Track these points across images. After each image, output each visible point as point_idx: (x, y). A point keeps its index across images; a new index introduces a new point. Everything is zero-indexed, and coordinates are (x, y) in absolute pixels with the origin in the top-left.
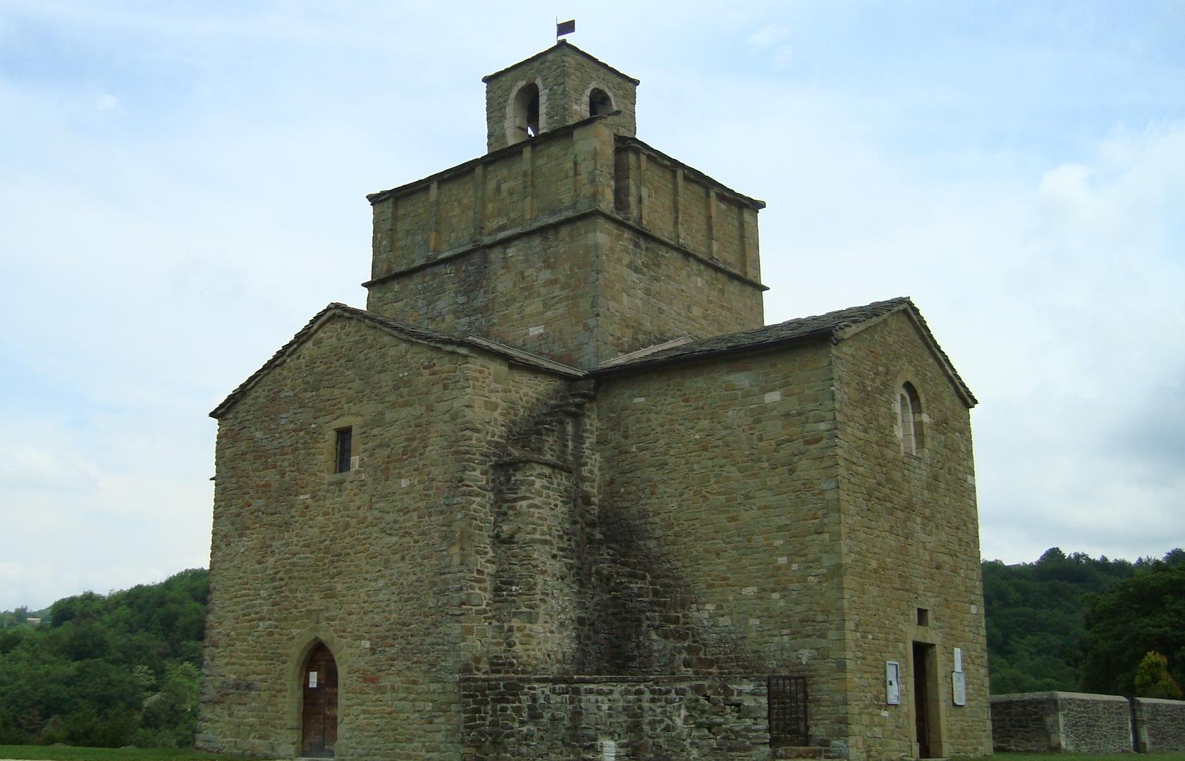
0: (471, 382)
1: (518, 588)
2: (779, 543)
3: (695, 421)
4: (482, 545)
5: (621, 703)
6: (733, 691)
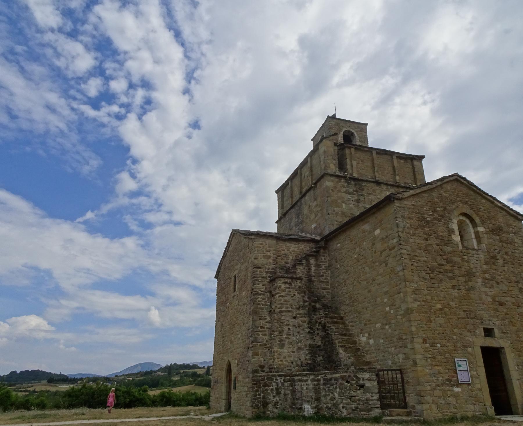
0: (256, 249)
2: (385, 300)
4: (263, 316)
6: (360, 378)
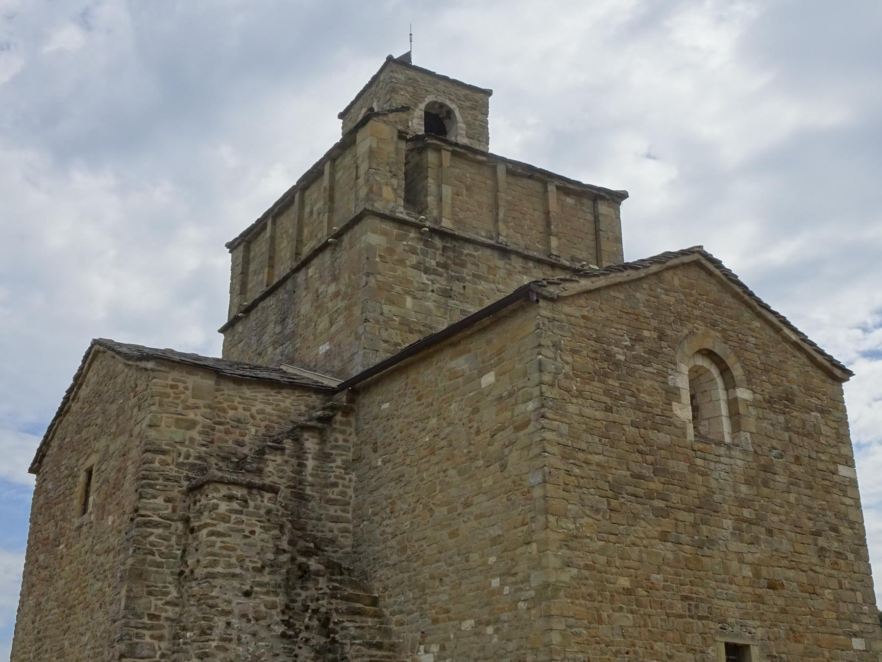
4: (160, 585)
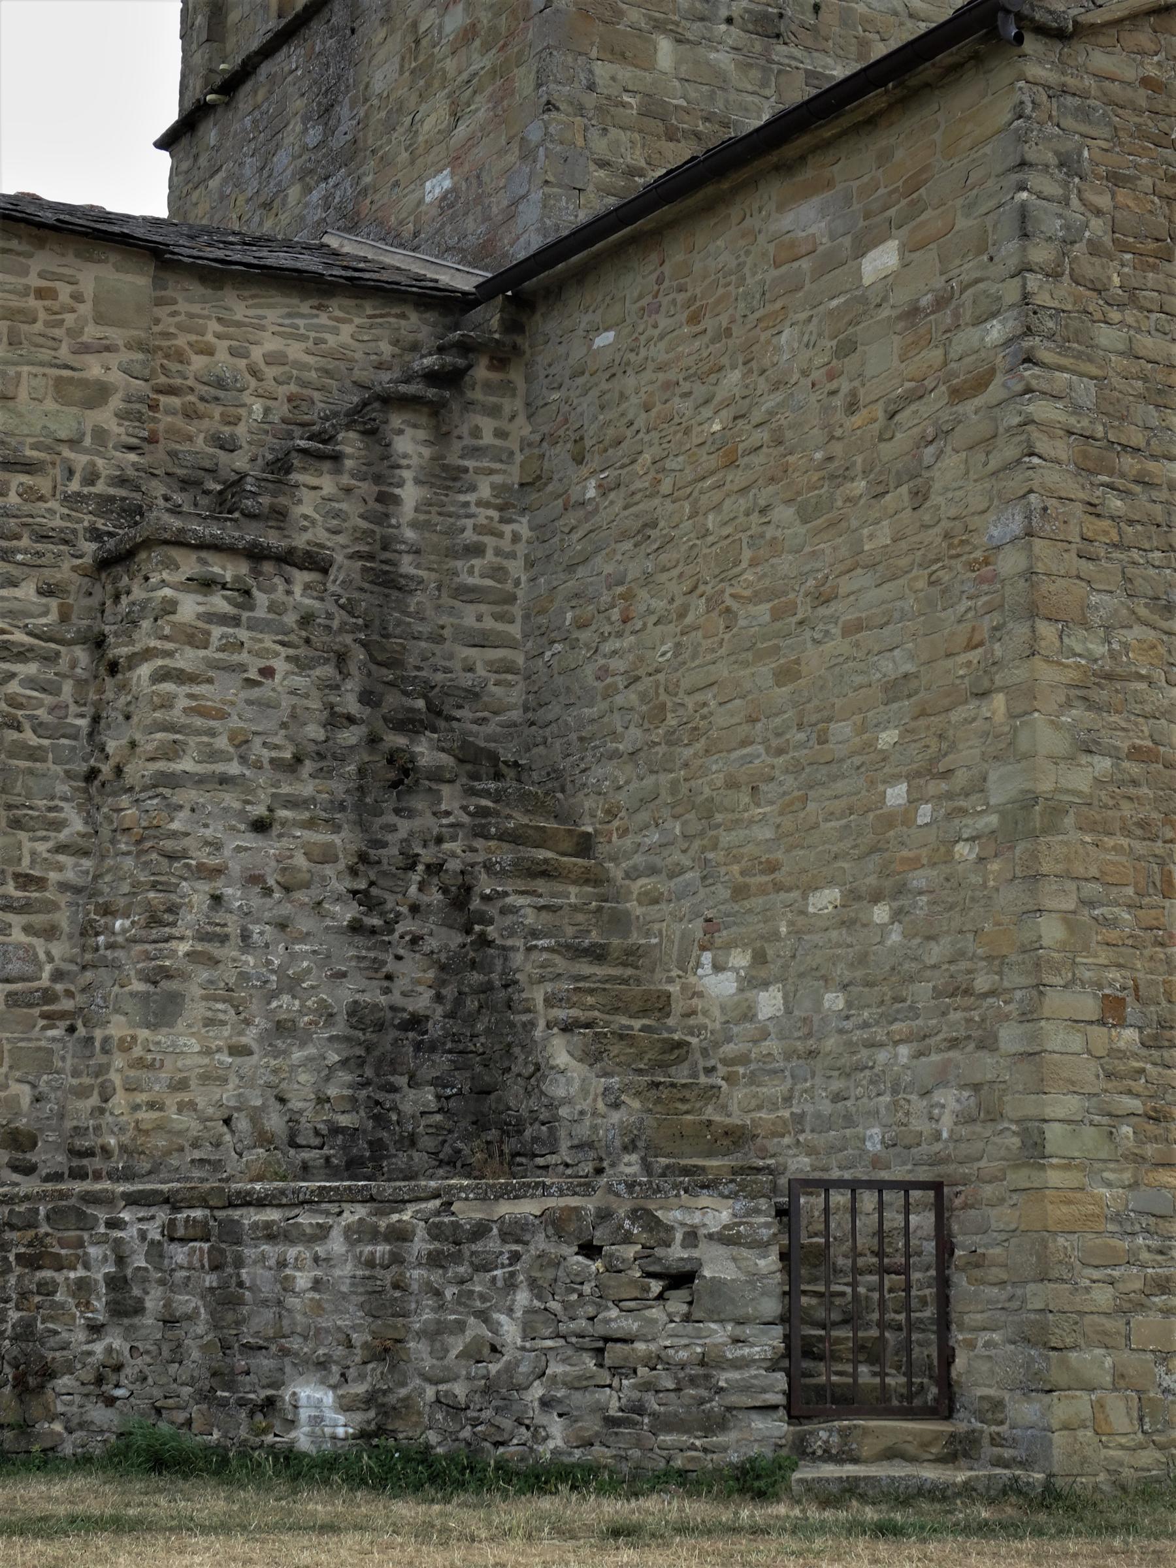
1: (127, 923)
3: (713, 378)
5: (348, 1269)
6: (670, 1229)
